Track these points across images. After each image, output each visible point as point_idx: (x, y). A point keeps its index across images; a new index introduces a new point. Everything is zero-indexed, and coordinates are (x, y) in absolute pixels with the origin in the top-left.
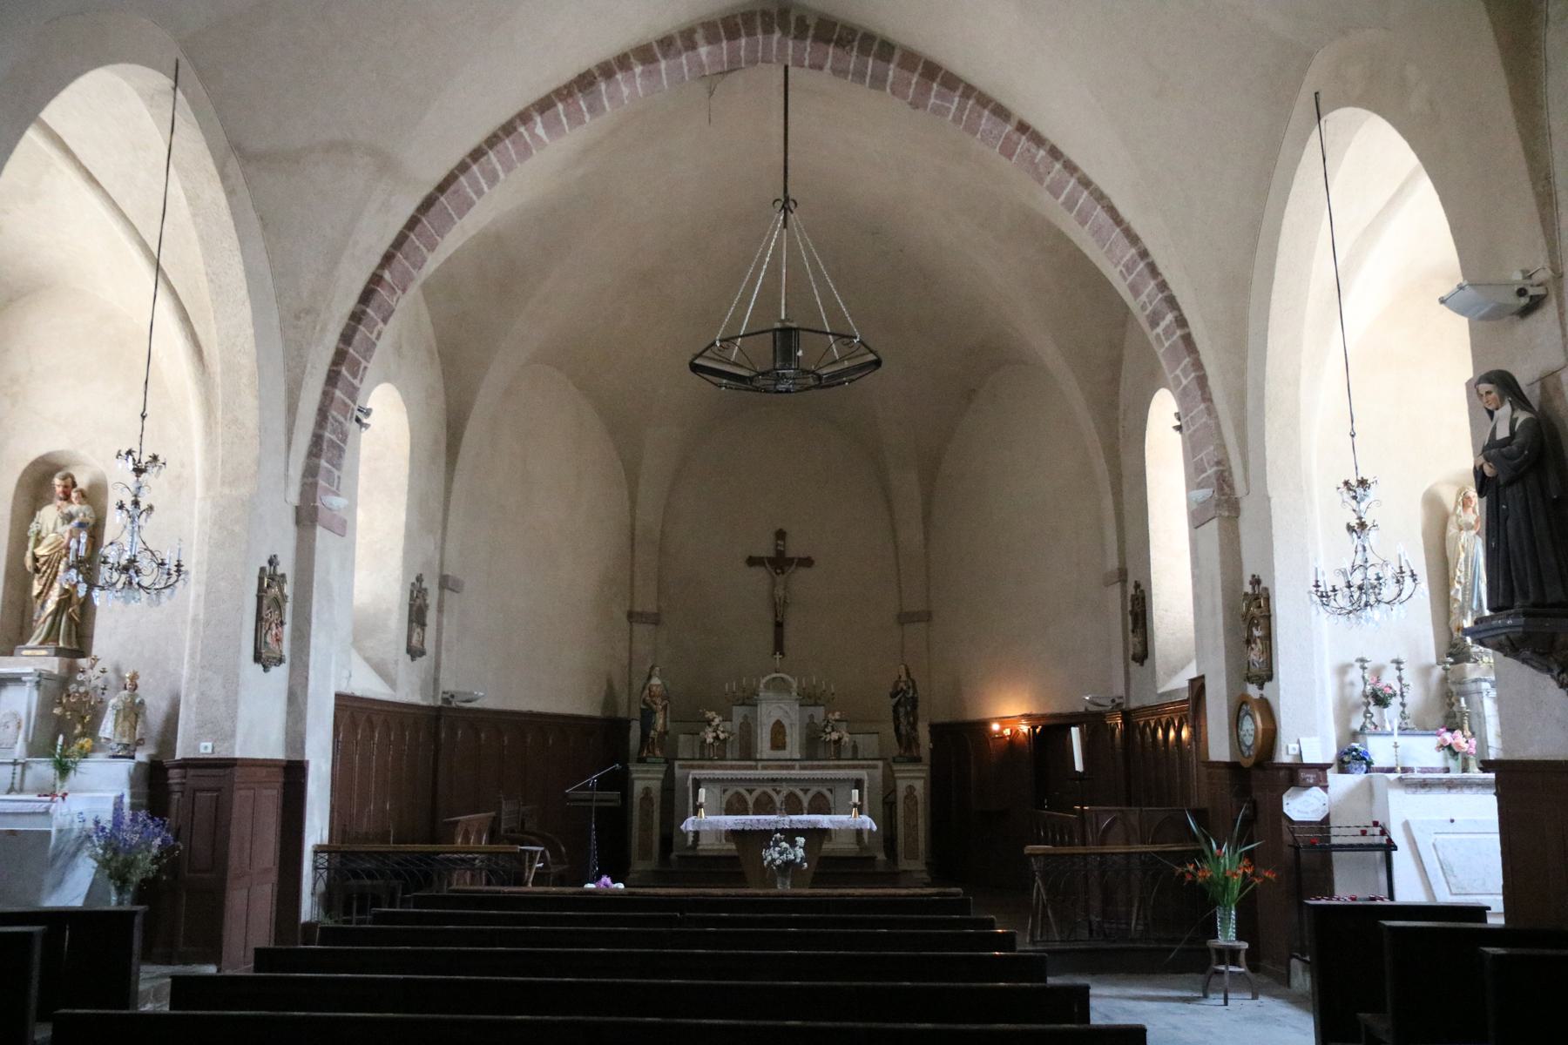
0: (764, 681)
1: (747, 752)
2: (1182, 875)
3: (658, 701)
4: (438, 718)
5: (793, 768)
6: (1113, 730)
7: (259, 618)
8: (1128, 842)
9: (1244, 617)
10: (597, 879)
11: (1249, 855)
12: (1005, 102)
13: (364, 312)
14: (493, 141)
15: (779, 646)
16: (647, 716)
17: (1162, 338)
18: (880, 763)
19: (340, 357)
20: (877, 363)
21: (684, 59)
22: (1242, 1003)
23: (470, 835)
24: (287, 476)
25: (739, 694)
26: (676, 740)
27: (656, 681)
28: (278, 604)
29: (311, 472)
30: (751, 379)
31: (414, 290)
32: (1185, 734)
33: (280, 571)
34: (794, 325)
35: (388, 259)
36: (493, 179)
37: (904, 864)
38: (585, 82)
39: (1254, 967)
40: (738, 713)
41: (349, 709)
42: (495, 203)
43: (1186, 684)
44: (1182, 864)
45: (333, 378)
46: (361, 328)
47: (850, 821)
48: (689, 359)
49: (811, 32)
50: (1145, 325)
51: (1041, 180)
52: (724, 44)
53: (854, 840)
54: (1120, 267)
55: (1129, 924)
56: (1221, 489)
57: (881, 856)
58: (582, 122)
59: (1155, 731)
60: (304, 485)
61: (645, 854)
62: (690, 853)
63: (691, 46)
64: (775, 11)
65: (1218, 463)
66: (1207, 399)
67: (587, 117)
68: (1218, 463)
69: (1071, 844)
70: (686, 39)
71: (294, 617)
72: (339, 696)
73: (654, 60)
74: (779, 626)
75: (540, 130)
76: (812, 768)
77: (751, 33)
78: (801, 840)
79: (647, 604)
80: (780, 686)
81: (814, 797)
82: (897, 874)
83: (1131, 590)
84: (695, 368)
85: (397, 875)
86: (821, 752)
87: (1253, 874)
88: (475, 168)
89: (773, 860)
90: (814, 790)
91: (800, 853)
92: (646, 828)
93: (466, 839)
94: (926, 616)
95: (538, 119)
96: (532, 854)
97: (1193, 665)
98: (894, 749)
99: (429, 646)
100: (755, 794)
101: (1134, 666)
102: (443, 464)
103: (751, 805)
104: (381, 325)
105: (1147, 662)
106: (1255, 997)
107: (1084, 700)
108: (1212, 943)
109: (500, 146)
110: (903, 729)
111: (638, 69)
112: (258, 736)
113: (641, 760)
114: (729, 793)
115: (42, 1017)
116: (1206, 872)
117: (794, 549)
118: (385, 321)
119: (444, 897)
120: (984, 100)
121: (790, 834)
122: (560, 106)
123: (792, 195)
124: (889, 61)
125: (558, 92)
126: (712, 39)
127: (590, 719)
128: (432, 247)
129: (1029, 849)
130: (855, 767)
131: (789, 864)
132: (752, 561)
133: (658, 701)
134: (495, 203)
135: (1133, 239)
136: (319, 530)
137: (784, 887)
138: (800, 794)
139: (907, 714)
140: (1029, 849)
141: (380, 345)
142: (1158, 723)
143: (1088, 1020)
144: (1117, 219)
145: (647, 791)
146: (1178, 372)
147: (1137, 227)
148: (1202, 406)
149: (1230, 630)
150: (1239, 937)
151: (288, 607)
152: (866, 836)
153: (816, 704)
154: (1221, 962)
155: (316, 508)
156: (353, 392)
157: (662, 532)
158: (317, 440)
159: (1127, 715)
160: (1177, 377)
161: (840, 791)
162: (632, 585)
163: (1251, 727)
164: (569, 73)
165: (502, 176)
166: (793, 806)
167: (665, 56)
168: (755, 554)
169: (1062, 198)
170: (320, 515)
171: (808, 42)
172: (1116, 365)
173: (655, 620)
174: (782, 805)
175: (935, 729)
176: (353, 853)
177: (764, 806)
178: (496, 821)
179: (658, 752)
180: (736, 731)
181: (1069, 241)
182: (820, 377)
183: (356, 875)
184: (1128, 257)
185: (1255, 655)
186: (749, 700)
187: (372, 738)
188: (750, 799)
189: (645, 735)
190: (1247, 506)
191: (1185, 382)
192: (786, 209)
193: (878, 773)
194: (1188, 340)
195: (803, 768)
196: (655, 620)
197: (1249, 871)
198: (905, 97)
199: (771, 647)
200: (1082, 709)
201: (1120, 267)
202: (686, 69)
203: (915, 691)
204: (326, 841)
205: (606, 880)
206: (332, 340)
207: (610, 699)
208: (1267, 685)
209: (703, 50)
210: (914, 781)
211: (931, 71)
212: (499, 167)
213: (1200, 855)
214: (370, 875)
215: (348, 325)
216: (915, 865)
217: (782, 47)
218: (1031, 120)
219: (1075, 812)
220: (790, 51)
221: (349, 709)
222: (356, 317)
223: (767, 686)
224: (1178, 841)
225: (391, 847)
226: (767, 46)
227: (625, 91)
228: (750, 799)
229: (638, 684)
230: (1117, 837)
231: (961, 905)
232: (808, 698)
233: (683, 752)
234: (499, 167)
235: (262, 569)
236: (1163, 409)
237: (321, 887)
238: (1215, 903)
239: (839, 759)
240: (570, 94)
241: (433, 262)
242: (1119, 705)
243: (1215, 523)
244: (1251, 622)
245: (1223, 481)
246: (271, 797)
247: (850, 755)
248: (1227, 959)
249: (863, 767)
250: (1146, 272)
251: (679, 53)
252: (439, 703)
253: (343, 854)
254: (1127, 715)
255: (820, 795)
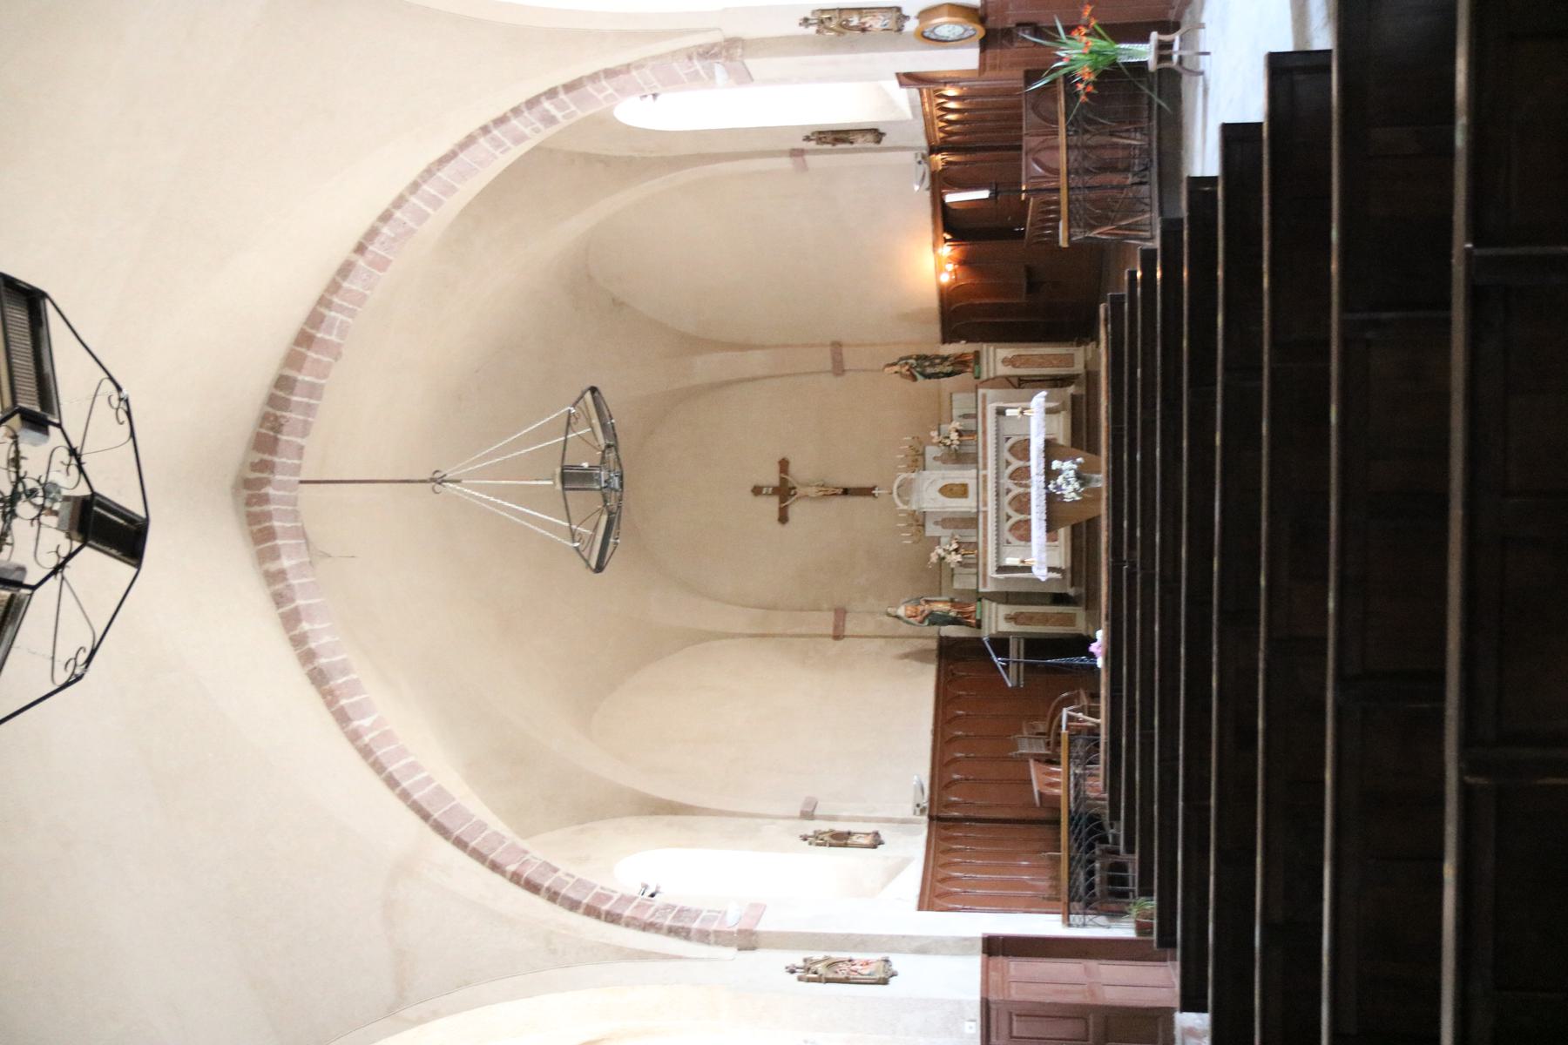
0: (902, 506)
1: (971, 521)
2: (1088, 94)
3: (920, 608)
4: (939, 819)
5: (985, 477)
6: (949, 163)
7: (846, 981)
8: (1057, 148)
9: (840, 33)
10: (1092, 656)
11: (1069, 30)
12: (336, 264)
13: (548, 889)
14: (378, 767)
15: (867, 492)
16: (936, 619)
17: (567, 112)
18: (981, 391)
19: (592, 911)
20: (593, 390)
21: (295, 582)
22: (1207, 38)
23: (1052, 782)
24: (709, 959)
25: (913, 529)
26: (962, 592)
27: (901, 611)
28: (832, 964)
29: (704, 937)
30: (610, 513)
31: (524, 844)
32: (951, 92)
33: (801, 964)
34: (558, 470)
35: (495, 867)
36: (414, 768)
37: (1079, 368)
38: (319, 678)
39: (1176, 26)
40: (932, 530)
41: (934, 896)
42: (439, 768)
43: (904, 91)
44: (1077, 95)
45: (613, 918)
46: (563, 891)
47: (1037, 418)
48: (591, 573)
49: (266, 457)
50: (554, 129)
51: (411, 232)
52: (279, 542)
53: (1054, 417)
54: (497, 153)
55: (1135, 147)
56: (715, 56)
57: (1071, 390)
58: (357, 681)
59: (950, 122)
60: (717, 943)
61: (1070, 620)
62: (1069, 576)
63: (280, 575)
64: (246, 493)
65: (690, 58)
66: (627, 68)
67: (354, 676)
68: (690, 58)
69: (1057, 203)
70: (274, 577)
71: (843, 950)
72: (920, 908)
73: (296, 611)
74: (846, 492)
75: (366, 722)
76: (985, 457)
77: (268, 516)
78: (1056, 465)
79: (826, 622)
80: (906, 489)
81: (1014, 455)
82: (1088, 373)
83: (812, 145)
84: (599, 568)
85: (1091, 847)
86: (971, 449)
87: (1087, 26)
88: (405, 784)
89: (1075, 491)
90: (1007, 455)
91: (1068, 465)
92: (1045, 619)
93: (1056, 785)
94: (837, 346)
95: (356, 724)
96: (1070, 718)
97: (883, 83)
98: (966, 378)
99: (870, 828)
100: (1011, 512)
101: (885, 142)
102: (695, 818)
103: (1022, 517)
104: (559, 874)
105: (882, 130)
106: (1202, 26)
107: (920, 192)
108: (1152, 66)
109: (384, 760)
110: (949, 369)
111: (305, 626)
112: (963, 979)
113: (979, 625)
114: (1011, 538)
115: (1098, 490)
116: (1085, 72)
117: (772, 478)
118: (555, 870)
119: (1111, 795)
120: (334, 287)
121: (1050, 474)
122: (343, 702)
123: (427, 476)
124: (295, 380)
125: (329, 705)
126: (274, 554)
127: (939, 671)
128: (482, 826)
129: (1063, 243)
130: (984, 416)
131: (1079, 476)
132: (783, 518)
133: (920, 608)
134: (439, 768)
135: (470, 140)
136: (760, 928)
137: (1101, 481)
138: (1011, 495)
139: (933, 365)
140: (1063, 243)
141: (578, 876)
142: (940, 118)
143: (1215, 178)
144: (451, 156)
145: (1009, 618)
146: (601, 97)
147: (460, 136)
148: (634, 73)
149: (852, 47)
150: (1146, 40)
151: (836, 955)
152: (1052, 405)
153: (923, 454)
154: (1169, 58)
155: (740, 932)
156: (626, 900)
157: (755, 607)
158: (673, 931)
159: (933, 150)
160: (606, 98)
161: (1008, 429)
162: (810, 636)
163: (948, 28)
164: (311, 693)
165: (411, 759)
166: (1022, 475)
167: (292, 600)
168: (776, 515)
169: (430, 210)
170: (744, 927)
171: (276, 459)
172: (588, 159)
173: (841, 613)
174: (1019, 485)
175: (948, 336)
176: (1070, 888)
177: (1022, 504)
178: (1038, 759)
179: (971, 608)
180: (949, 532)
181: (469, 204)
182: (608, 446)
183: (1091, 886)
184: (487, 146)
185: (876, 23)
186: (919, 520)
187: (958, 878)
188: (1016, 517)
189: (955, 621)
190: (732, 31)
191: (611, 91)
192: (441, 481)
193: (990, 393)
194: (569, 87)
195: (985, 467)
196: (841, 613)
197: (1084, 31)
198: (329, 366)
199: (869, 499)
200: (928, 194)
201: (497, 153)
202: (304, 580)
203: (910, 357)
204: (1059, 917)
205: (1093, 648)
206: (577, 920)
207: (920, 656)
208: (905, 12)
209: (286, 563)
210: (997, 358)
211: (305, 339)
212: (403, 762)
213: (1068, 78)
214: (1091, 873)
215: (561, 905)
216: (1077, 357)
217: (283, 486)
218: (352, 243)
219: (1027, 199)
220: (285, 478)
221: (934, 896)
222: (553, 896)
223: (906, 503)
224: (1055, 100)
225: (1064, 854)
226: (281, 500)
227: (326, 639)
228: (1016, 517)
229: (904, 629)
230: (1050, 160)
231: (1117, 303)
232: (917, 461)
233: (970, 583)
234: (403, 762)
235: (800, 979)
236: (634, 112)
237: (1102, 919)
238: (1114, 63)
239: (976, 432)
240: (331, 692)
241: (496, 825)
242: (923, 157)
243: (749, 62)
244: (845, 27)
245: (708, 53)
246: (1017, 967)
247: (972, 421)
248: (1166, 52)
249: (984, 408)
250: (503, 127)
251: (289, 587)
252: (925, 818)
253: (1071, 899)
254: (933, 150)
255: (1011, 449)
